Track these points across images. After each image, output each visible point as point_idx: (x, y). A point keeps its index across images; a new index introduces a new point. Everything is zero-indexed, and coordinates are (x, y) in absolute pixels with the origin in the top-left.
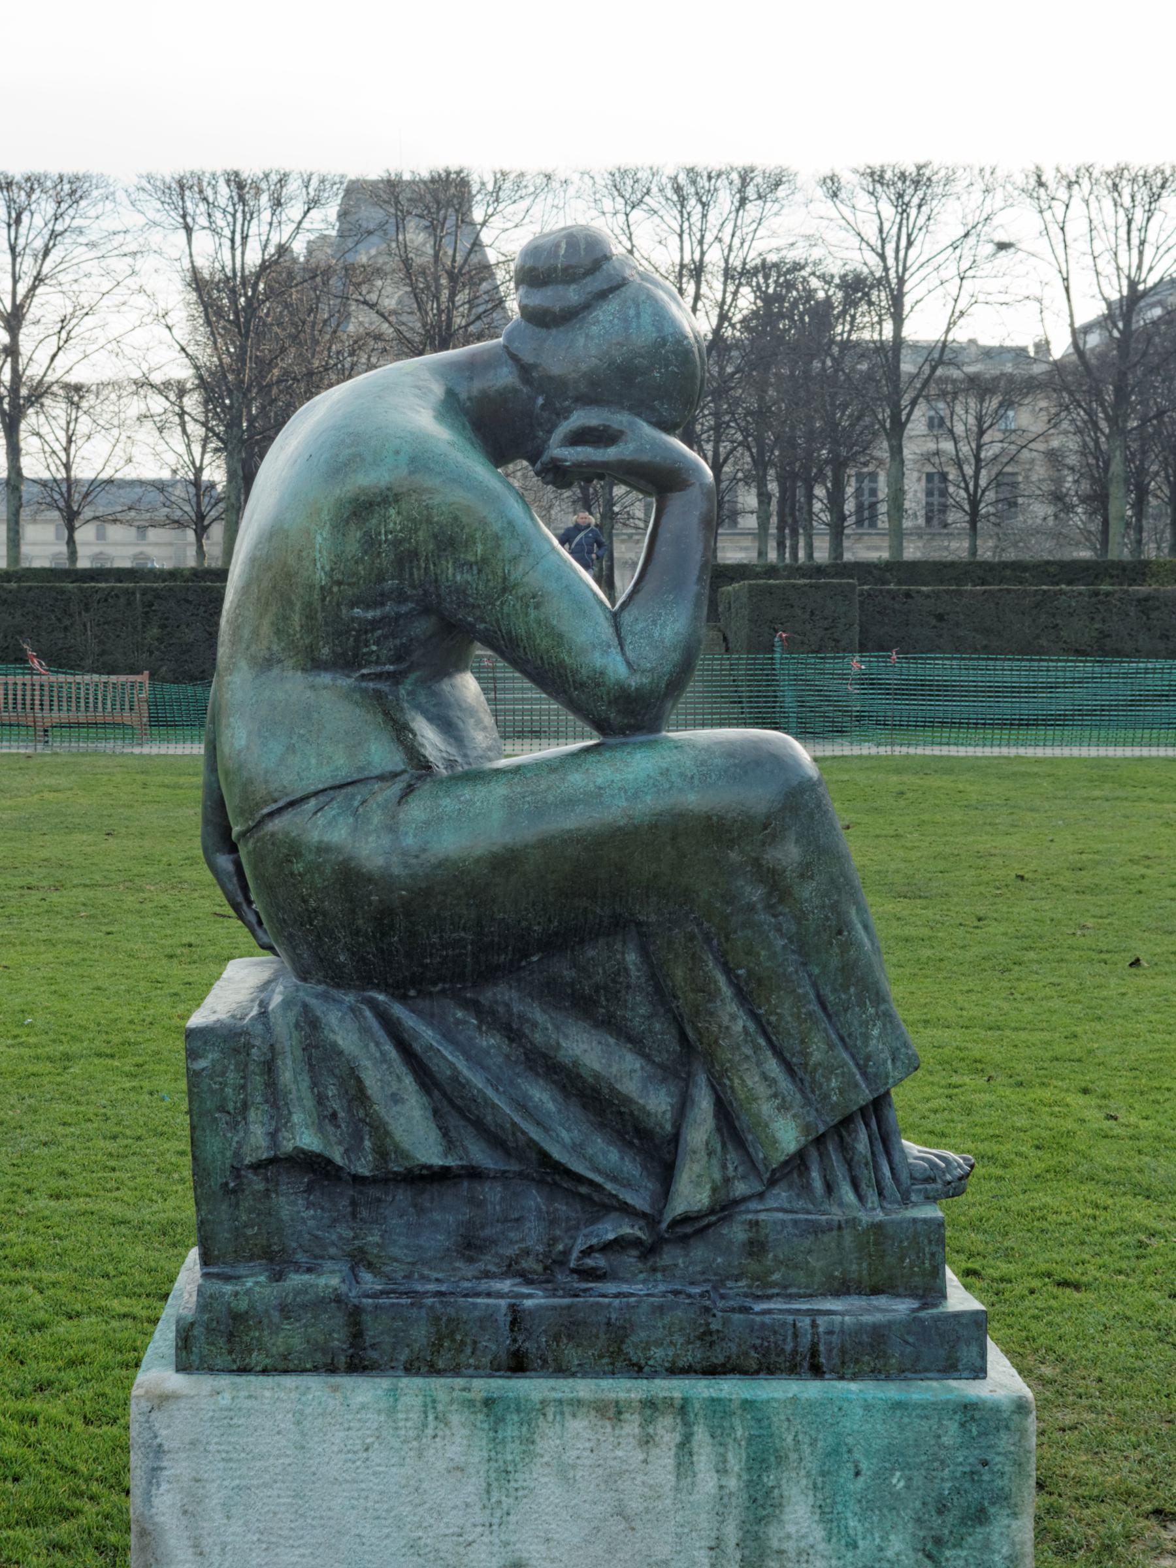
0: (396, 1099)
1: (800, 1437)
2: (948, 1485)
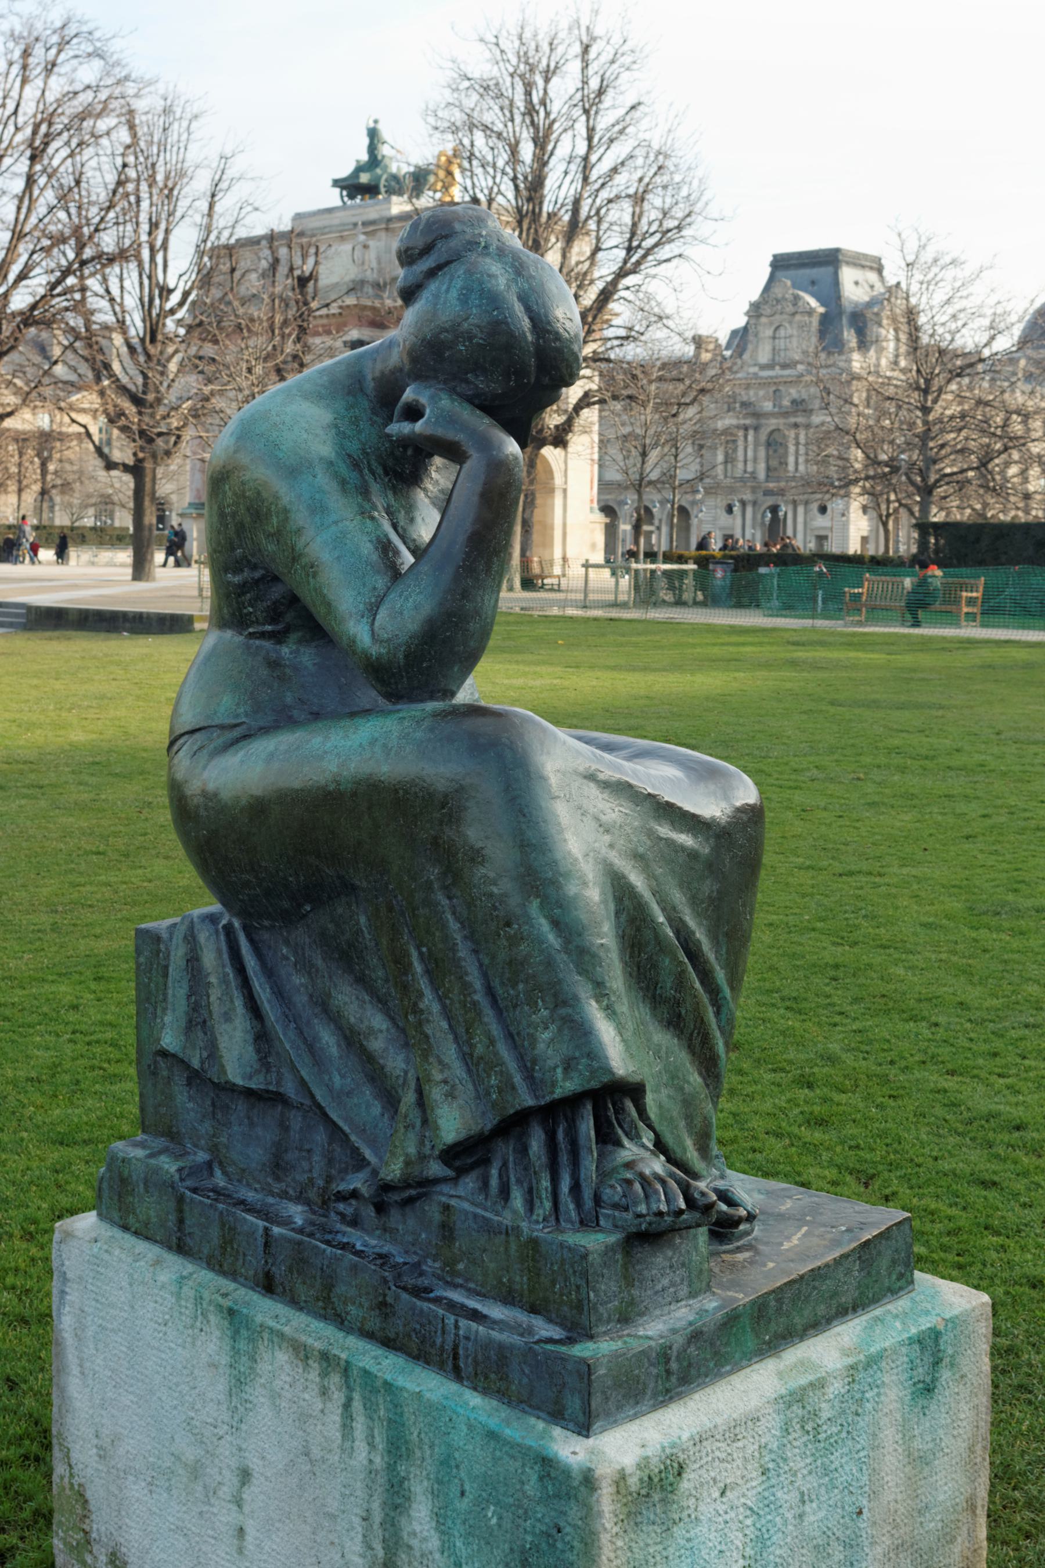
0: (227, 1017)
1: (423, 1436)
2: (529, 1538)
